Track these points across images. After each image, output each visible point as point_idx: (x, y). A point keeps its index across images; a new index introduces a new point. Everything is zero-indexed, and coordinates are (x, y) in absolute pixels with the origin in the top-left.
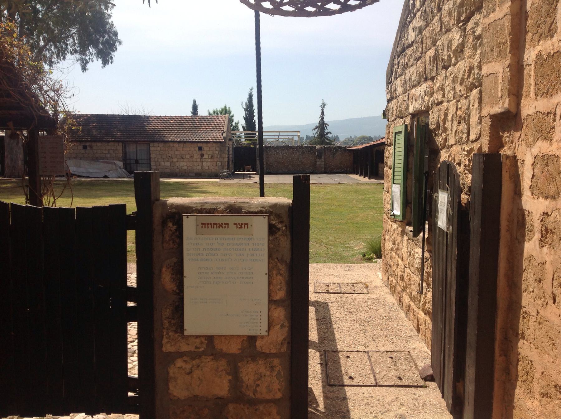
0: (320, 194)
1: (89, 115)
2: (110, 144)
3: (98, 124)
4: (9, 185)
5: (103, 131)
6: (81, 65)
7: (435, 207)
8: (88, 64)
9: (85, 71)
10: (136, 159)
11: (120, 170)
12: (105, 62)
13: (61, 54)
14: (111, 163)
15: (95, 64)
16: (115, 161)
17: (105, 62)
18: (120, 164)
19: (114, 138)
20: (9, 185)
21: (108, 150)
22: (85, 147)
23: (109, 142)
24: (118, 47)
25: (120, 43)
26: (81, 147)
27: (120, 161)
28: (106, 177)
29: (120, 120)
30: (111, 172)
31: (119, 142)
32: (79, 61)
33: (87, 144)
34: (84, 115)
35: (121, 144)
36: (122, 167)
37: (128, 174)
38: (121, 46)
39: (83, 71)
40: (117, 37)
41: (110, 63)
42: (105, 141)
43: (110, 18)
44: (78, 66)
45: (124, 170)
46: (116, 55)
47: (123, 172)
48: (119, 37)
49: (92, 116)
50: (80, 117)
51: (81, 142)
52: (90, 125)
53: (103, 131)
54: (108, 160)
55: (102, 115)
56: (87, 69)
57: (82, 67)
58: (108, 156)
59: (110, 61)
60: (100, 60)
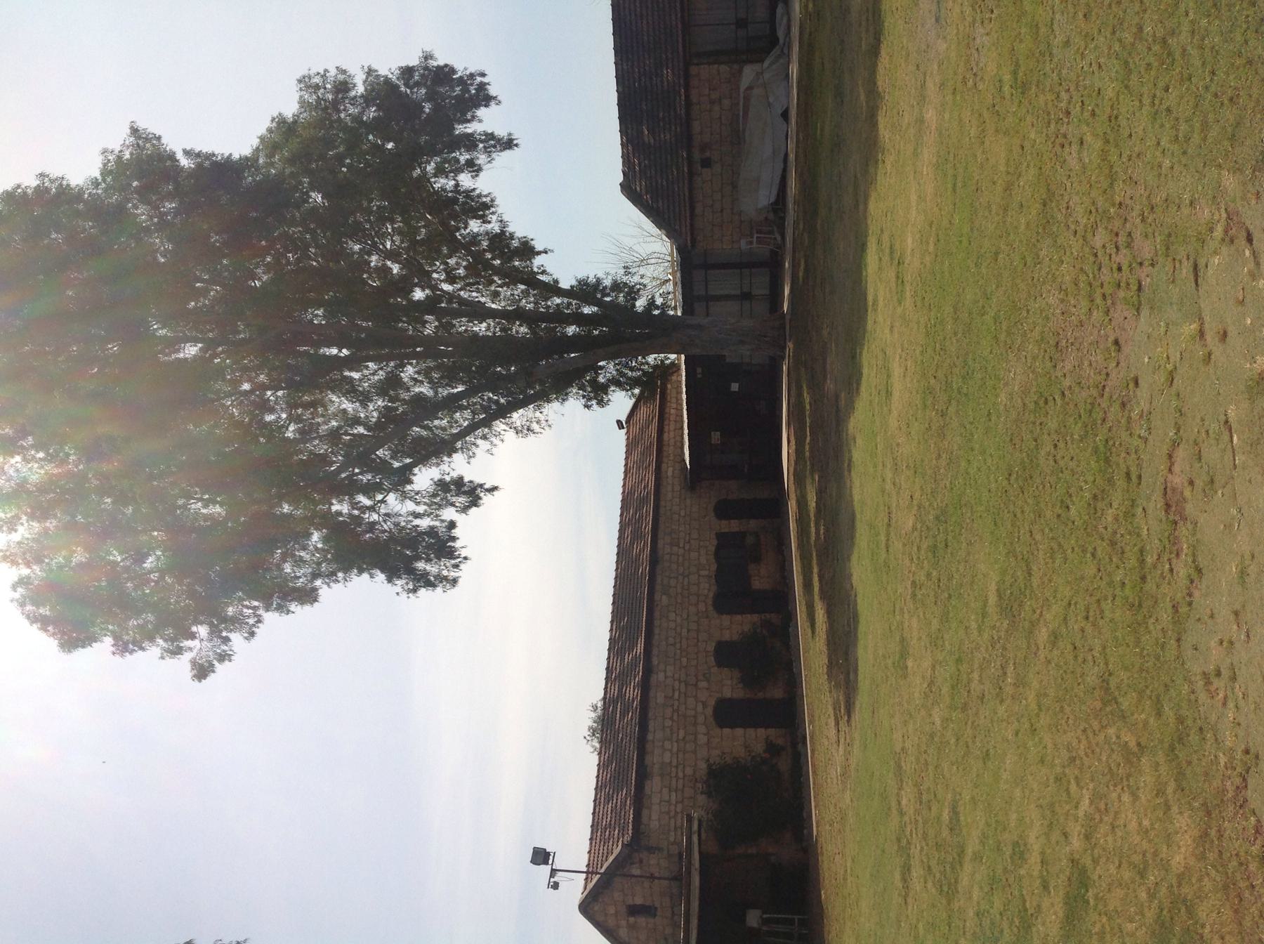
0: (887, 331)
1: (622, 138)
2: (694, 99)
3: (645, 122)
4: (807, 398)
5: (661, 115)
6: (501, 151)
7: (639, 801)
8: (496, 134)
9: (515, 142)
10: (733, 27)
11: (767, 76)
12: (484, 98)
13: (480, 207)
14: (747, 99)
15: (487, 121)
16: (742, 90)
17: (484, 98)
18: (749, 72)
19: (677, 88)
20: (807, 398)
21: (712, 102)
22: (706, 163)
23: (689, 104)
24: (441, 63)
25: (427, 57)
26: (706, 172)
27: (740, 71)
28: (785, 115)
29: (630, 63)
30: (771, 100)
31: (687, 76)
32: (494, 155)
33: (697, 156)
34: (623, 152)
35: (694, 70)
36: (757, 67)
37: (776, 51)
38: (436, 55)
39: (516, 145)
40: (414, 67)
41: (485, 80)
42: (688, 113)
43: (376, 71)
44: (503, 158)
45: (766, 64)
46: (463, 64)
47: (771, 65)
48: (414, 61)
49: (623, 131)
50: (629, 161)
51: (691, 174)
52: (646, 139)
53: (661, 115)
54: (738, 104)
55: (619, 104)
56: (510, 134)
57: (505, 149)
58: (726, 102)
59: (479, 79)
60: (481, 112)
